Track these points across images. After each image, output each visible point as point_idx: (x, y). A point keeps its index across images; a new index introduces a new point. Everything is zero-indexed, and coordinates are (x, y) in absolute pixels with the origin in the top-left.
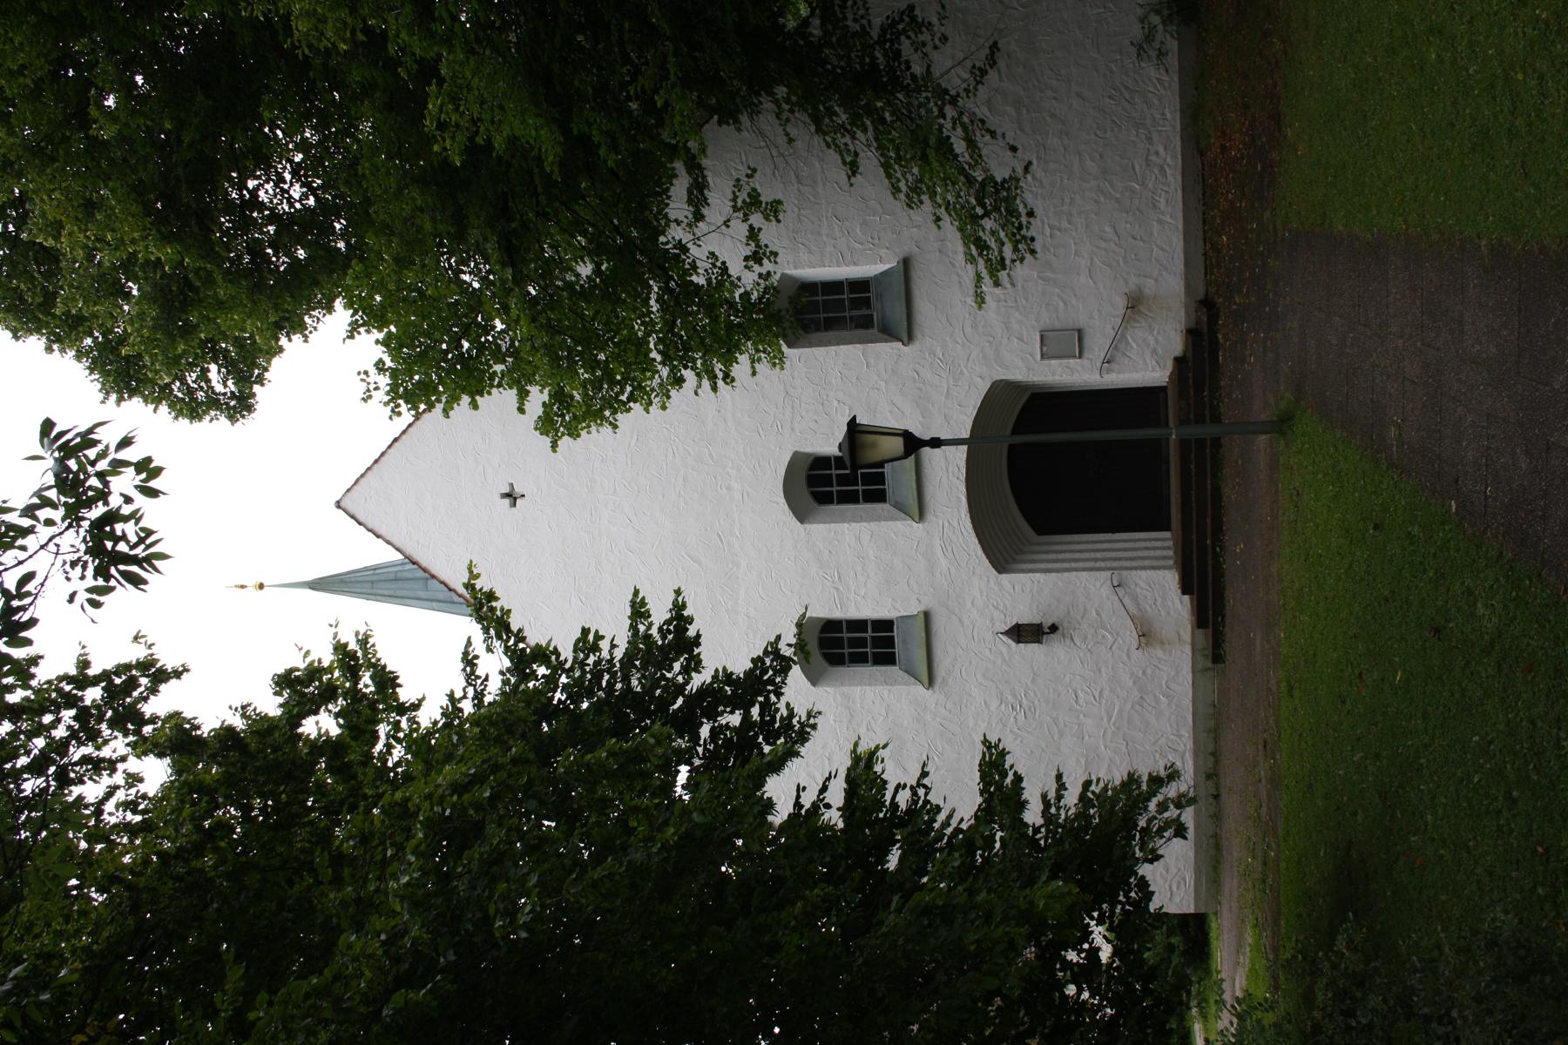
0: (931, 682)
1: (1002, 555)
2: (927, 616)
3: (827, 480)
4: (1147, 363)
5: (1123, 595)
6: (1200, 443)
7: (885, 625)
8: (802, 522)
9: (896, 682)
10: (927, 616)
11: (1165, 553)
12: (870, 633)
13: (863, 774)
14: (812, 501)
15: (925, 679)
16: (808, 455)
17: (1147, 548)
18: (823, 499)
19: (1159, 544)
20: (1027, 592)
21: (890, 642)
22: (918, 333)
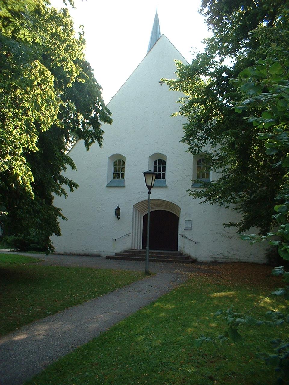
0: (107, 187)
1: (138, 207)
2: (167, 187)
3: (160, 164)
4: (184, 245)
5: (127, 234)
6: (145, 256)
7: (164, 177)
8: (150, 157)
9: (108, 178)
10: (124, 187)
11: (136, 247)
12: (121, 173)
13: (222, 168)
14: (115, 160)
15: (108, 186)
16: (166, 160)
17: (138, 243)
18: (115, 164)
19: (139, 245)
20: (128, 212)
21: (119, 177)
22: (107, 188)
